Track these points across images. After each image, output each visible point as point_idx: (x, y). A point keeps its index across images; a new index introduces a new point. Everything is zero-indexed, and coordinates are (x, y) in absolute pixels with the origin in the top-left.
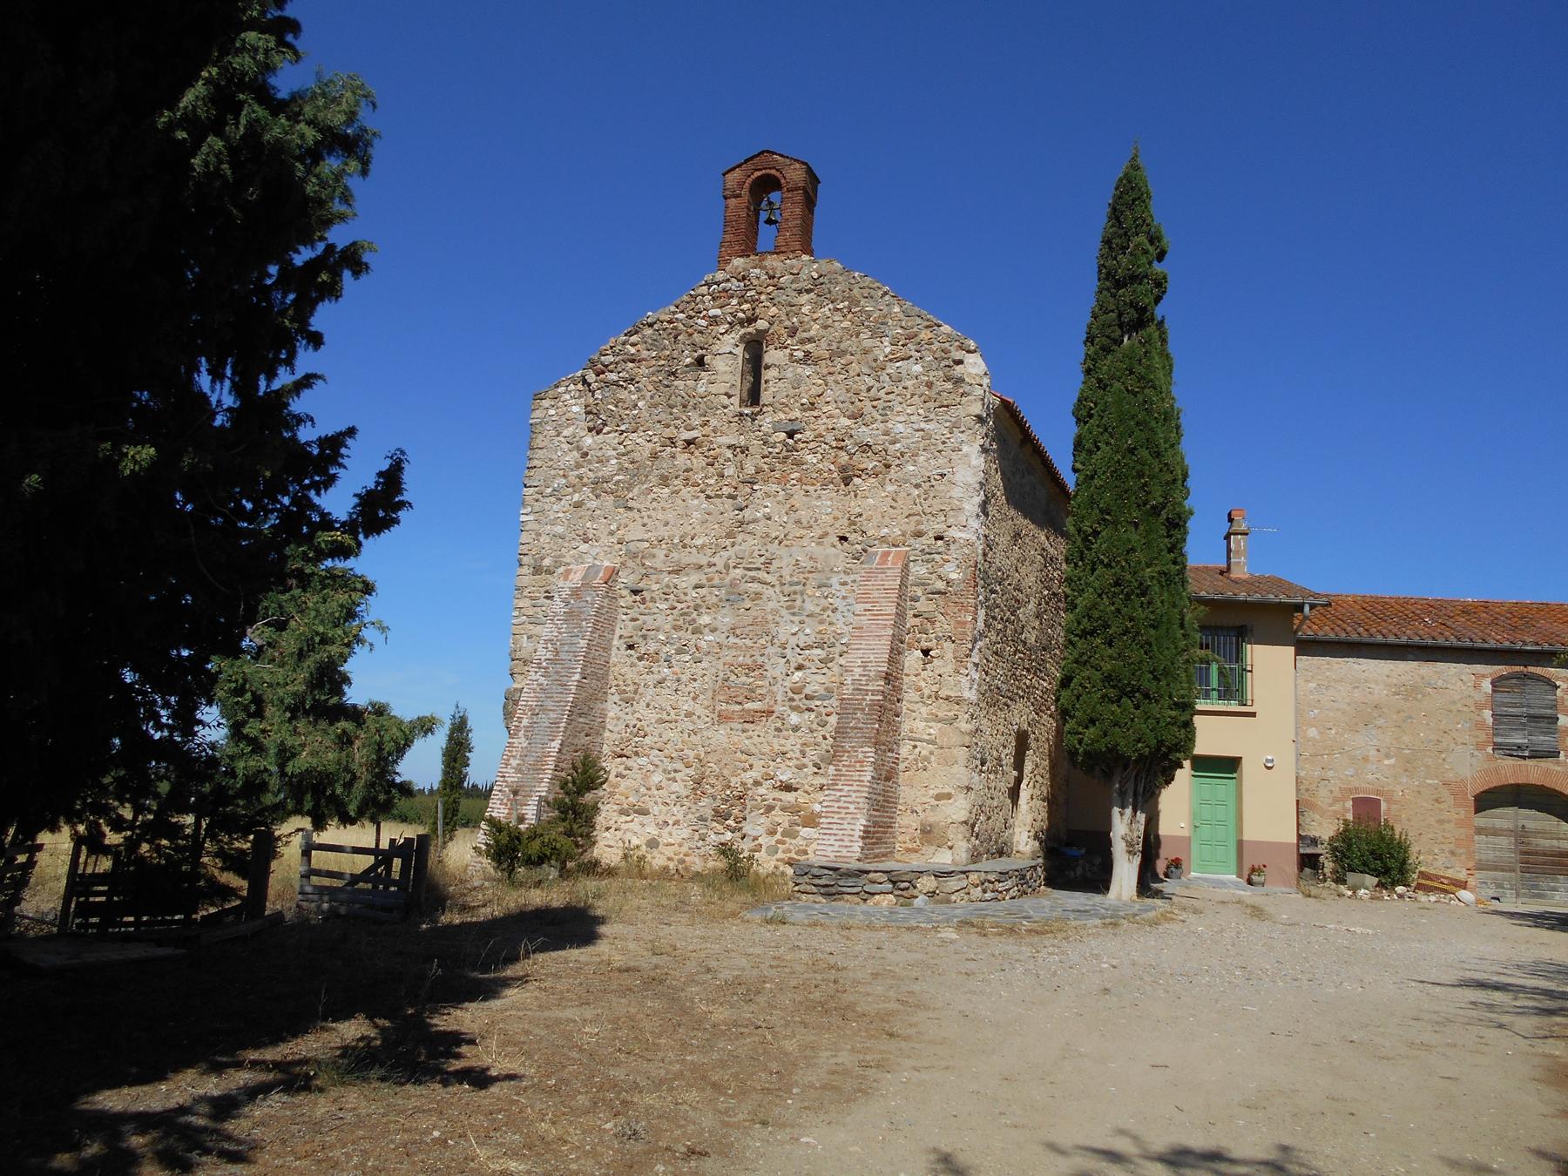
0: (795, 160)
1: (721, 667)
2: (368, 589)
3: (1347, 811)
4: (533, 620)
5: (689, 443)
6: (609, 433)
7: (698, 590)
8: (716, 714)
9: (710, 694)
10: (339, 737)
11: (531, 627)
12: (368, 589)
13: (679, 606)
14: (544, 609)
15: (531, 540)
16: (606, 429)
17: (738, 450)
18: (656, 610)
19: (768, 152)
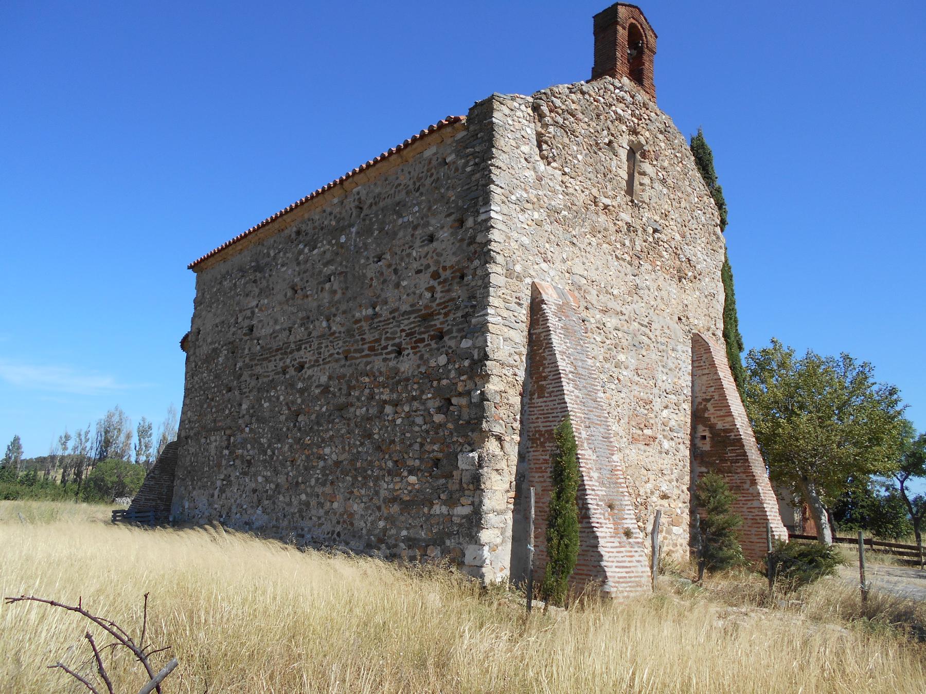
0: (652, 29)
1: (632, 398)
2: (893, 391)
3: (808, 533)
4: (507, 323)
5: (606, 207)
6: (555, 168)
7: (617, 332)
8: (631, 436)
9: (626, 419)
10: (801, 410)
11: (506, 329)
12: (893, 391)
13: (608, 342)
14: (516, 314)
15: (502, 241)
16: (554, 164)
17: (632, 228)
18: (592, 340)
19: (639, 9)
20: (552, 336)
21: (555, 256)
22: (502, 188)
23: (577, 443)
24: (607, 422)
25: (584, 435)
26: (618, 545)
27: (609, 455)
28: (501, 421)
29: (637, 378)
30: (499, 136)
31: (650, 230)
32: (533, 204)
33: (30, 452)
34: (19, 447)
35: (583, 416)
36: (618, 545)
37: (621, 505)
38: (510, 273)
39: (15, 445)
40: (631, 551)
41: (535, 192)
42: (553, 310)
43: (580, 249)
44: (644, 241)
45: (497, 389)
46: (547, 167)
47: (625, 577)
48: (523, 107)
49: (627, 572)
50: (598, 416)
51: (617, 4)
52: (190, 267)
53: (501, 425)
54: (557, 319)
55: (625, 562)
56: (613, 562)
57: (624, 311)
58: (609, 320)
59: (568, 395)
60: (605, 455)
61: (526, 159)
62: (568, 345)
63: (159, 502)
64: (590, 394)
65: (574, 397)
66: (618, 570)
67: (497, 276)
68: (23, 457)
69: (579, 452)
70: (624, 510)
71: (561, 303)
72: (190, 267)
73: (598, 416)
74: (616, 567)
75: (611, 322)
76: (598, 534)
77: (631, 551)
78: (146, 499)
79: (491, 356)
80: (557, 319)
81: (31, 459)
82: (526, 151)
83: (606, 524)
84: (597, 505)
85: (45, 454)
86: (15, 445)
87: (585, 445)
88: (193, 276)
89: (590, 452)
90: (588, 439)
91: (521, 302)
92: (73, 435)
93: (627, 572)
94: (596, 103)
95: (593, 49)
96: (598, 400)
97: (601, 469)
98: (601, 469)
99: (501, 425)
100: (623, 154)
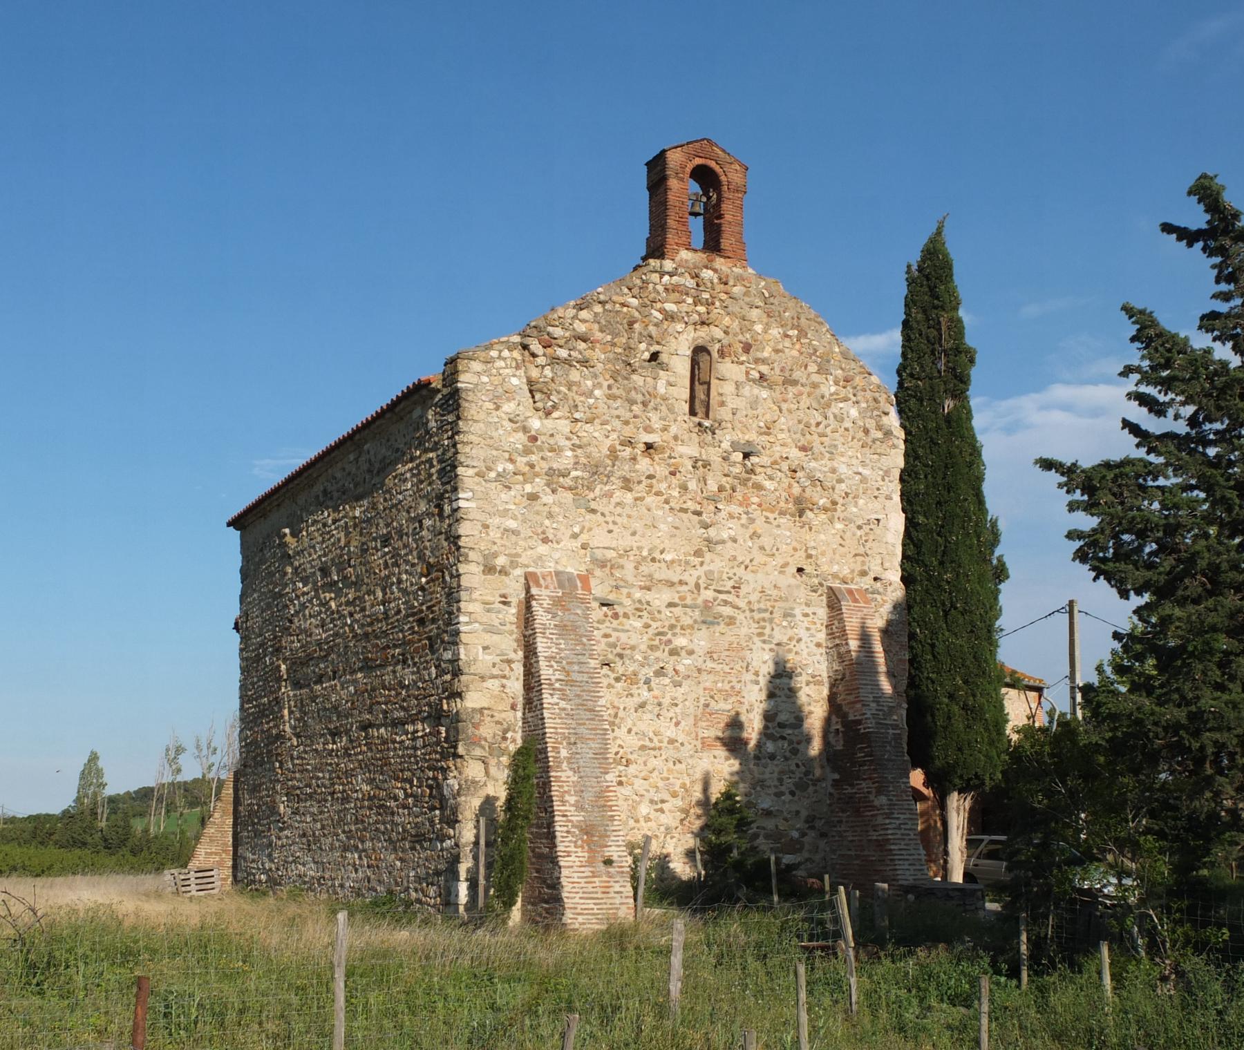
5: (649, 446)
7: (672, 609)
20: (538, 640)
21: (559, 534)
22: (474, 467)
23: (551, 764)
24: (605, 734)
25: (564, 753)
26: (591, 874)
27: (599, 775)
28: (483, 743)
29: (710, 664)
30: (467, 405)
31: (738, 456)
32: (523, 474)
33: (119, 782)
34: (99, 773)
35: (567, 731)
36: (591, 874)
37: (606, 830)
38: (489, 569)
39: (91, 772)
40: (609, 882)
41: (525, 460)
42: (545, 606)
43: (603, 514)
44: (725, 475)
45: (477, 706)
46: (545, 421)
47: (593, 909)
48: (506, 353)
49: (595, 904)
50: (591, 729)
51: (664, 152)
52: (229, 524)
53: (483, 748)
54: (550, 616)
55: (597, 893)
56: (577, 893)
57: (686, 577)
58: (657, 596)
59: (548, 709)
60: (594, 775)
61: (510, 420)
62: (563, 646)
63: (224, 855)
64: (587, 707)
65: (557, 711)
66: (582, 901)
67: (471, 573)
68: (109, 791)
69: (552, 774)
70: (609, 836)
71: (560, 594)
72: (229, 524)
73: (591, 729)
74: (581, 898)
75: (658, 599)
76: (562, 864)
77: (609, 882)
78: (206, 853)
79: (466, 670)
80: (550, 616)
81: (128, 793)
82: (509, 411)
83: (576, 852)
84: (568, 832)
85: (988, 505)
86: (91, 772)
87: (565, 764)
88: (235, 535)
89: (570, 773)
90: (569, 758)
91: (509, 600)
92: (189, 744)
93: (595, 904)
94: (625, 309)
95: (239, 541)
96: (597, 709)
97: (582, 791)
98: (582, 791)
99: (483, 748)
100: (682, 367)
